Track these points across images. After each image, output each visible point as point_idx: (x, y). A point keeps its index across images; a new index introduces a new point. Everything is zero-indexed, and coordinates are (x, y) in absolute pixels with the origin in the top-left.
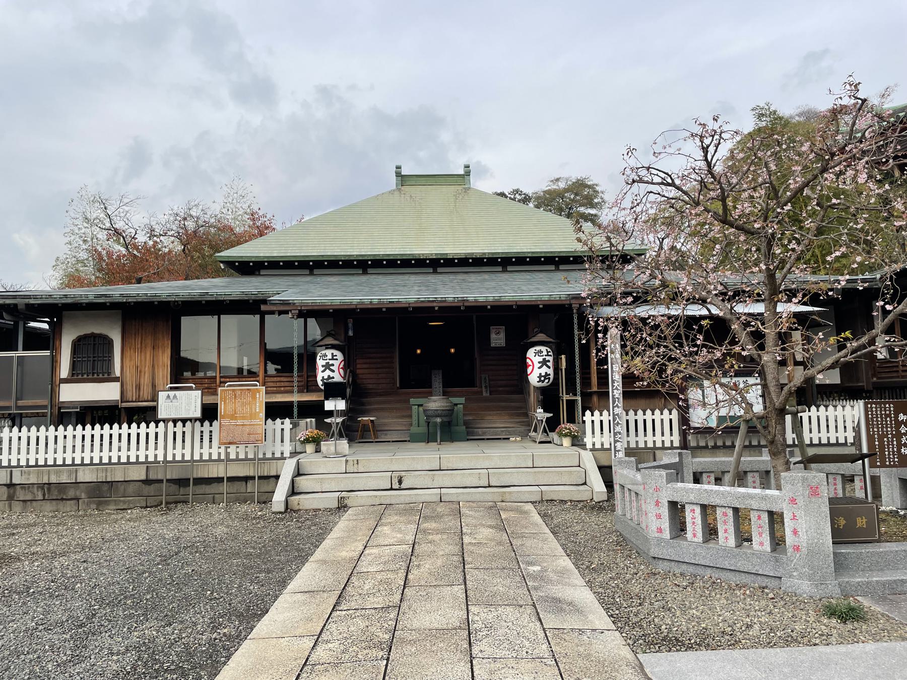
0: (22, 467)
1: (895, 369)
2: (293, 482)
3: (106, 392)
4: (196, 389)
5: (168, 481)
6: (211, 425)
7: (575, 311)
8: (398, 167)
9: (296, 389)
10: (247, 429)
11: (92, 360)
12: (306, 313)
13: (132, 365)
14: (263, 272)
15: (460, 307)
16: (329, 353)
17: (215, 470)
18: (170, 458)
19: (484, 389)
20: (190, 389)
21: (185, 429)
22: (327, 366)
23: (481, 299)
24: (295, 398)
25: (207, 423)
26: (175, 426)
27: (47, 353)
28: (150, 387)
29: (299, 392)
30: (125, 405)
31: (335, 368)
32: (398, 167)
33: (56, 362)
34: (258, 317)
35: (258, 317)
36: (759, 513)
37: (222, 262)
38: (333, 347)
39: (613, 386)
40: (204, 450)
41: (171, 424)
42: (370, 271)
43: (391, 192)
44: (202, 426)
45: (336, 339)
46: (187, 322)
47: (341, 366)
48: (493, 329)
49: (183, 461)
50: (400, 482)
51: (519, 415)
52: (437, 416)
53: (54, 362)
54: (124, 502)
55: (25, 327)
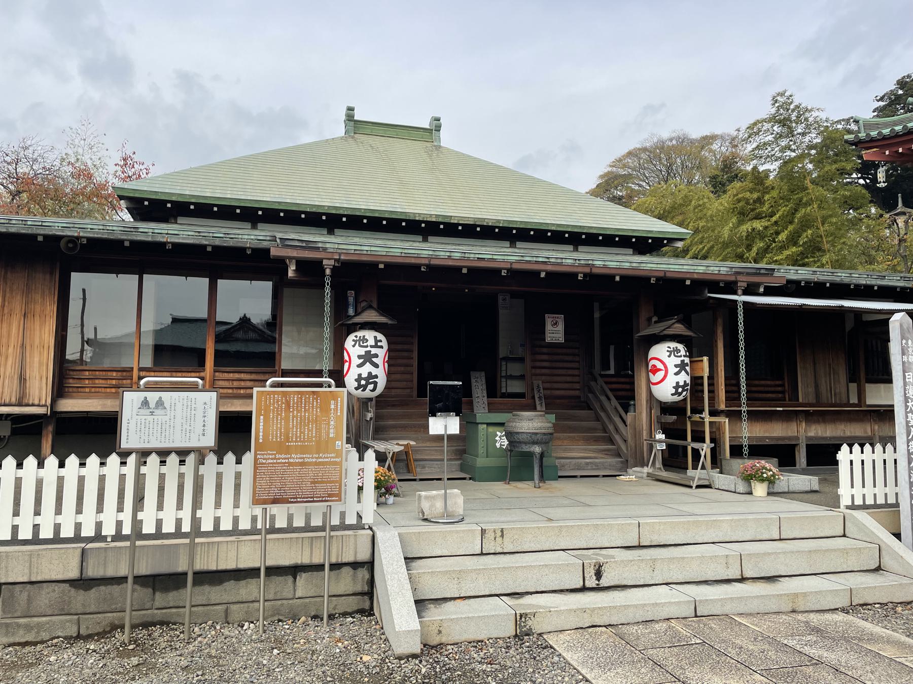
5: (138, 579)
8: (351, 109)
17: (232, 554)
19: (538, 402)
20: (193, 388)
21: (164, 469)
25: (230, 457)
28: (16, 382)
40: (226, 509)
43: (342, 138)
48: (549, 320)
50: (598, 575)
51: (597, 440)
54: (28, 628)
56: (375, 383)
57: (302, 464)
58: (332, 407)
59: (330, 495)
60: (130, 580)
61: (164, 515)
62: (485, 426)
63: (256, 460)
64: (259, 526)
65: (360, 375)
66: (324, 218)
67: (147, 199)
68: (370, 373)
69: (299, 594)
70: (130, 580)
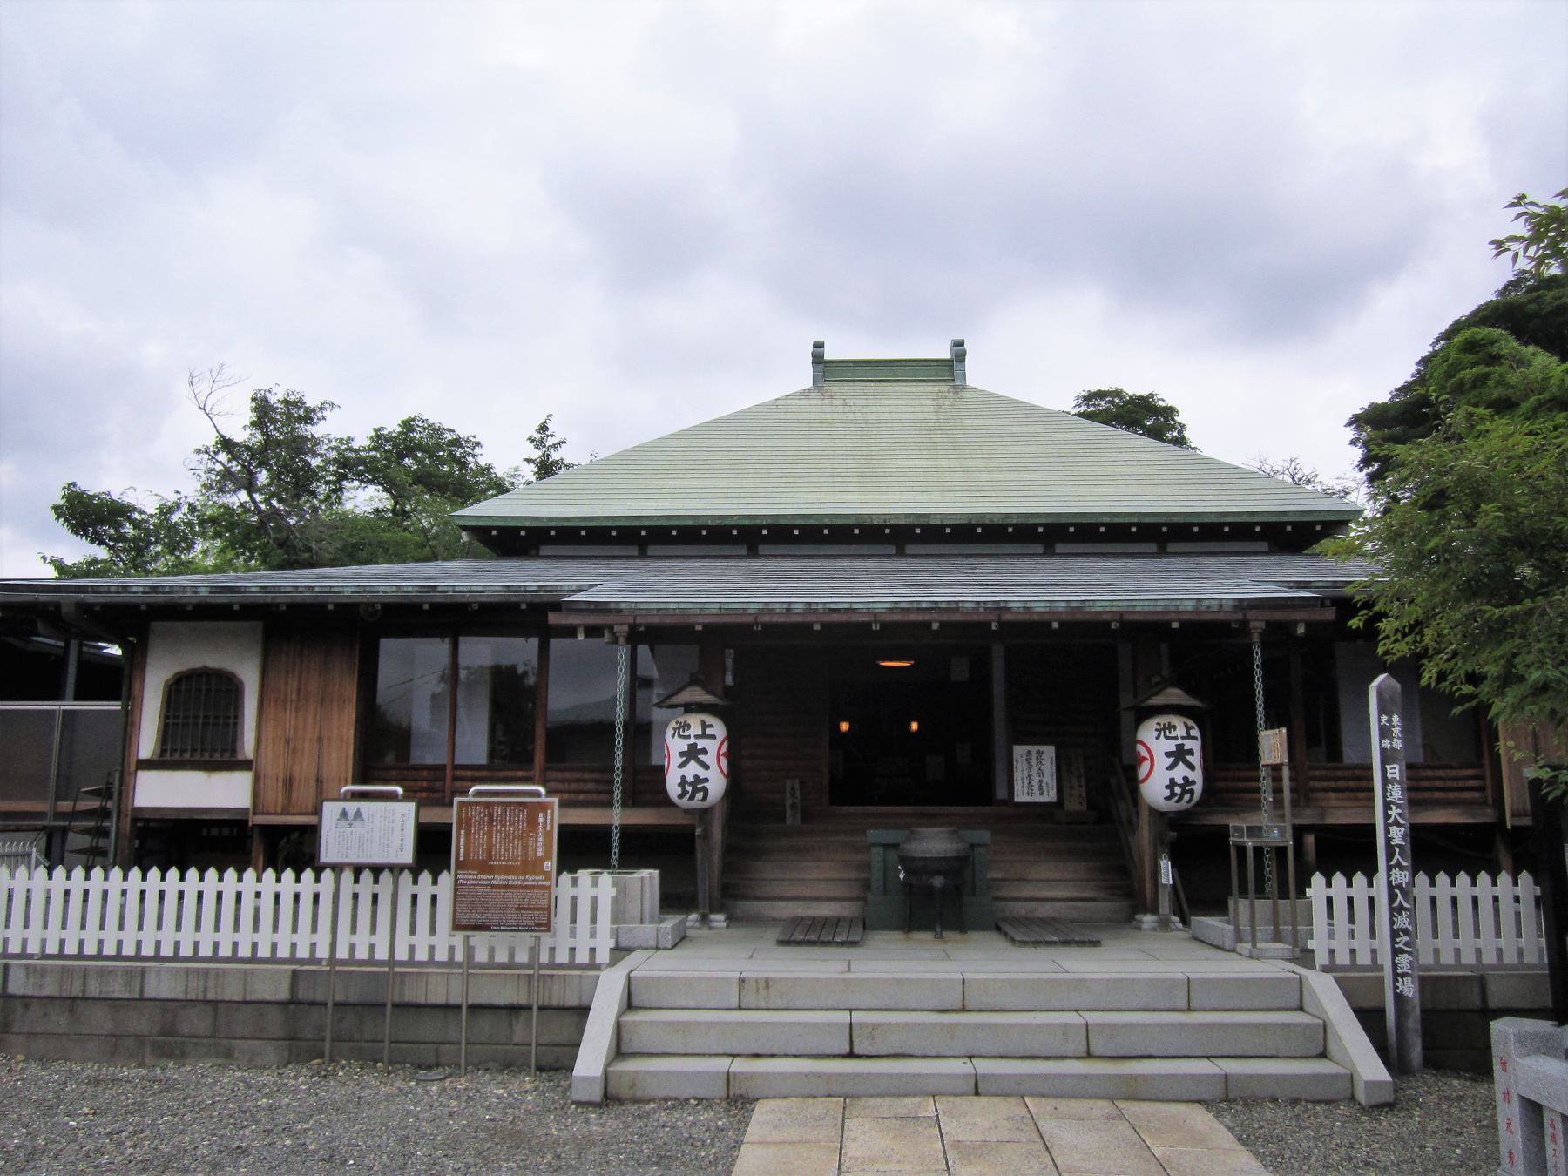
0: (31, 956)
2: (619, 1027)
3: (225, 792)
4: (406, 798)
6: (435, 882)
7: (1256, 638)
9: (617, 797)
10: (516, 897)
11: (201, 730)
12: (655, 633)
13: (287, 732)
14: (545, 550)
15: (988, 624)
16: (695, 721)
18: (343, 953)
20: (391, 797)
22: (692, 754)
23: (1039, 607)
24: (617, 817)
25: (426, 877)
26: (357, 881)
27: (115, 706)
30: (260, 820)
31: (709, 759)
32: (819, 345)
33: (133, 724)
34: (534, 642)
35: (534, 642)
37: (464, 528)
38: (701, 708)
39: (1387, 817)
40: (417, 934)
41: (347, 876)
42: (763, 549)
43: (804, 394)
44: (415, 882)
45: (709, 692)
46: (391, 649)
47: (724, 749)
49: (371, 961)
52: (939, 873)
53: (128, 725)
55: (80, 652)
56: (1192, 792)
57: (506, 887)
59: (538, 925)
61: (364, 942)
62: (881, 850)
63: (456, 880)
65: (1172, 780)
67: (826, 526)
68: (1185, 778)
69: (516, 1039)
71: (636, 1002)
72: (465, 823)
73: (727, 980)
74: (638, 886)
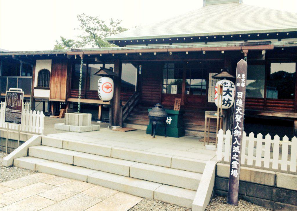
1: (77, 96)
29: (81, 98)
36: (66, 198)
56: (230, 103)
58: (20, 97)
59: (19, 122)
60: (18, 141)
64: (7, 128)
66: (192, 38)
68: (229, 99)
70: (18, 141)
71: (43, 143)
72: (8, 97)
73: (60, 140)
74: (77, 117)
